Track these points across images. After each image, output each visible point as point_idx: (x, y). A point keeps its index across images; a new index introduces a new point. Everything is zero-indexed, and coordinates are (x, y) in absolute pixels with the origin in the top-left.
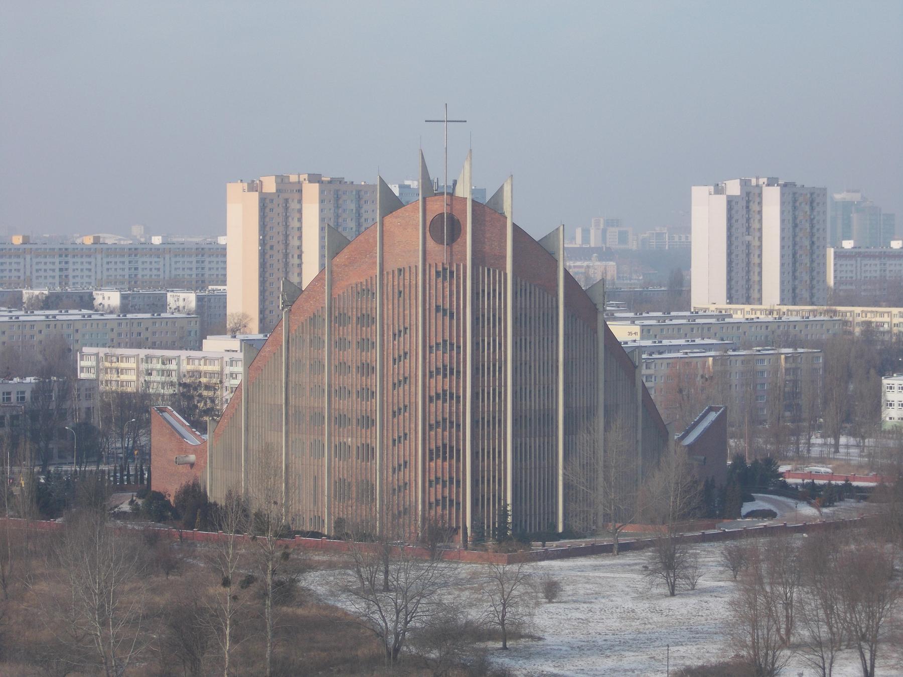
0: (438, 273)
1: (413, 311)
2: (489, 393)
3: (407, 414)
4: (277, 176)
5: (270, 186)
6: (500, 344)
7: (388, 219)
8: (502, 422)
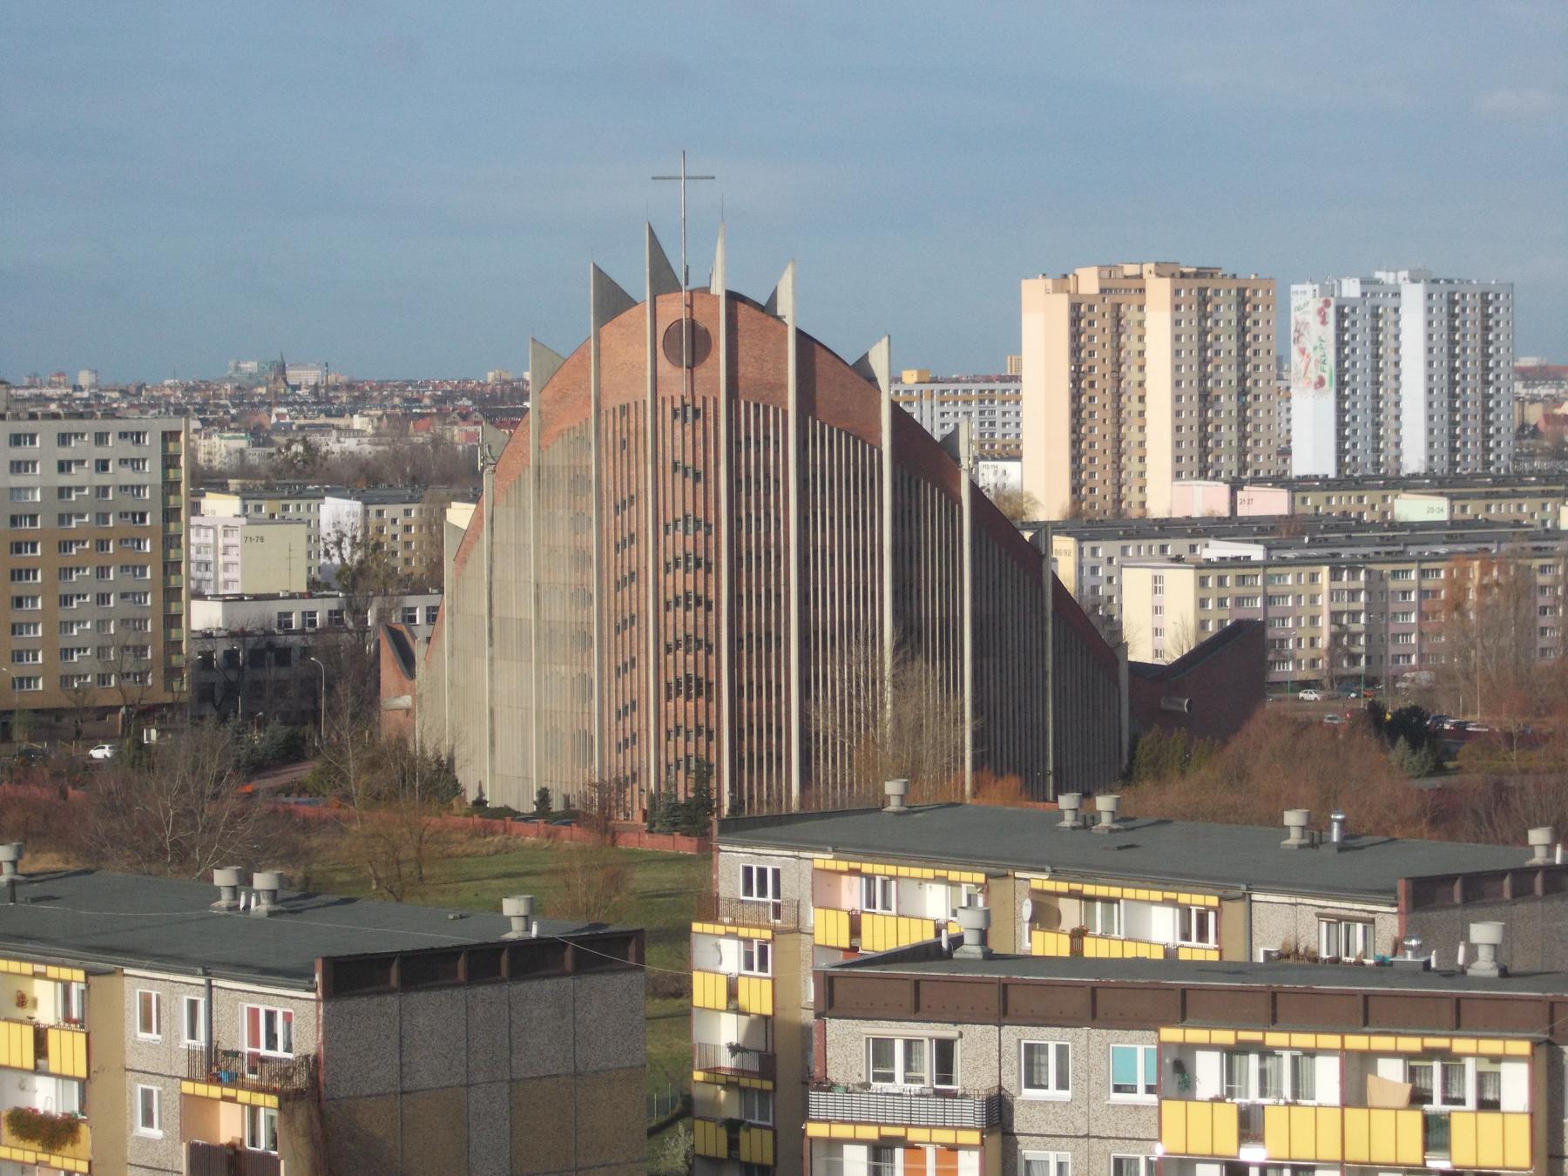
0: (675, 414)
1: (641, 470)
2: (759, 596)
3: (635, 628)
4: (1101, 267)
5: (1089, 282)
6: (777, 520)
7: (607, 330)
8: (781, 641)
